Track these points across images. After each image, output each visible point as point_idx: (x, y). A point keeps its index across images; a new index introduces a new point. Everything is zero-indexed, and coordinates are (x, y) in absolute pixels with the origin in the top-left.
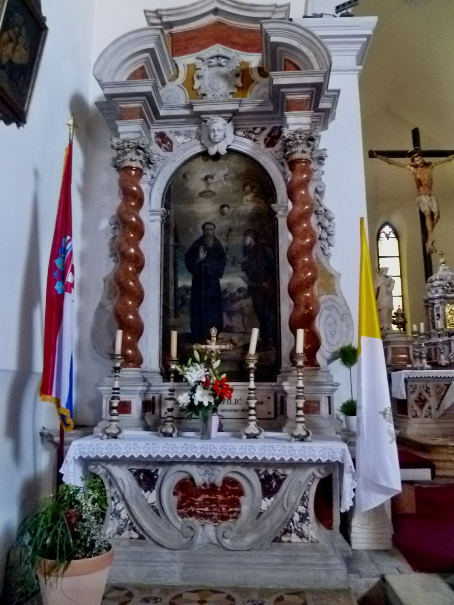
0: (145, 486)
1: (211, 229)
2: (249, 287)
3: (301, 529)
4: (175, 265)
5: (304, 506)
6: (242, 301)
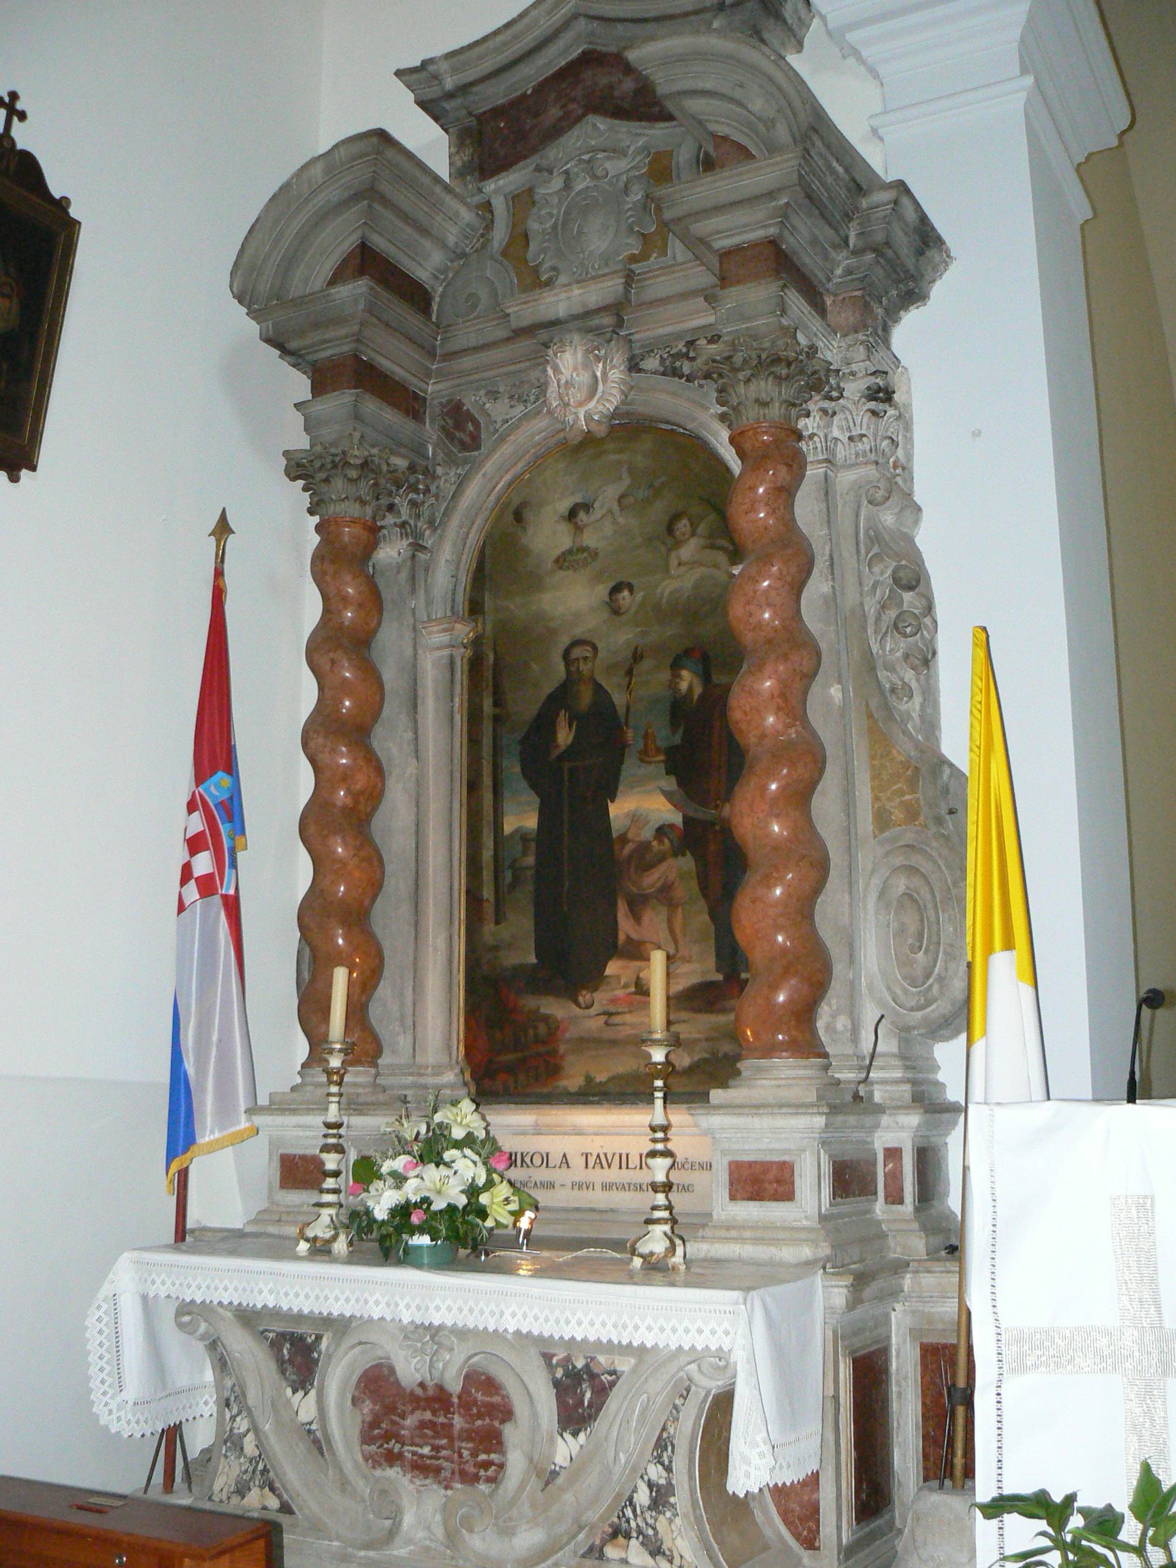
0: (294, 1377)
1: (586, 658)
2: (687, 820)
3: (654, 1529)
4: (496, 768)
5: (662, 1464)
6: (663, 867)
